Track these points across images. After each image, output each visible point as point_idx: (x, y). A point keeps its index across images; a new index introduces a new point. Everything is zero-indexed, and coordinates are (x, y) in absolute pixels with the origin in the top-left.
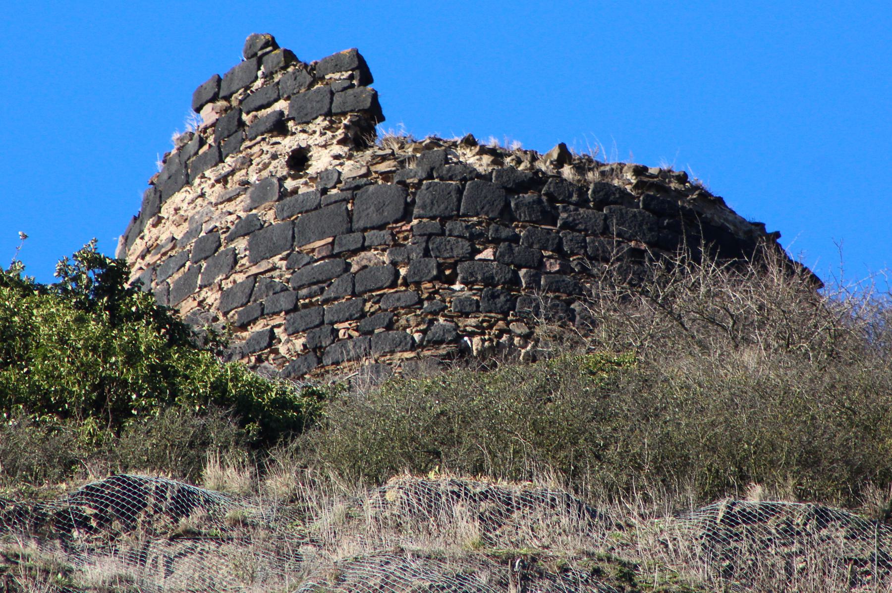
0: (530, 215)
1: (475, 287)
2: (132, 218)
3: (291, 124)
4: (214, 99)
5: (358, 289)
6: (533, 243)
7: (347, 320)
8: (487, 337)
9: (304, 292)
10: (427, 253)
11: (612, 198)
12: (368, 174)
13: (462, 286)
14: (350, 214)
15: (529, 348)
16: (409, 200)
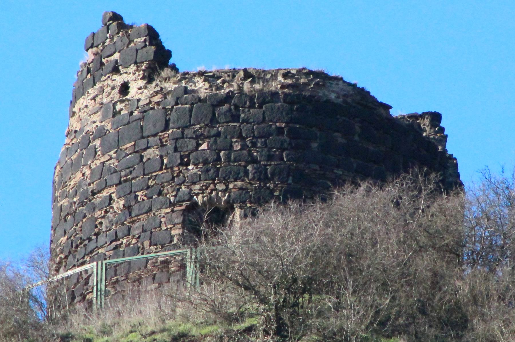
0: (226, 119)
1: (199, 167)
2: (70, 102)
3: (120, 68)
4: (92, 47)
5: (146, 172)
6: (227, 135)
7: (141, 190)
8: (205, 195)
9: (123, 173)
10: (176, 150)
11: (267, 100)
12: (150, 102)
13: (193, 166)
14: (142, 127)
15: (226, 197)
16: (167, 119)
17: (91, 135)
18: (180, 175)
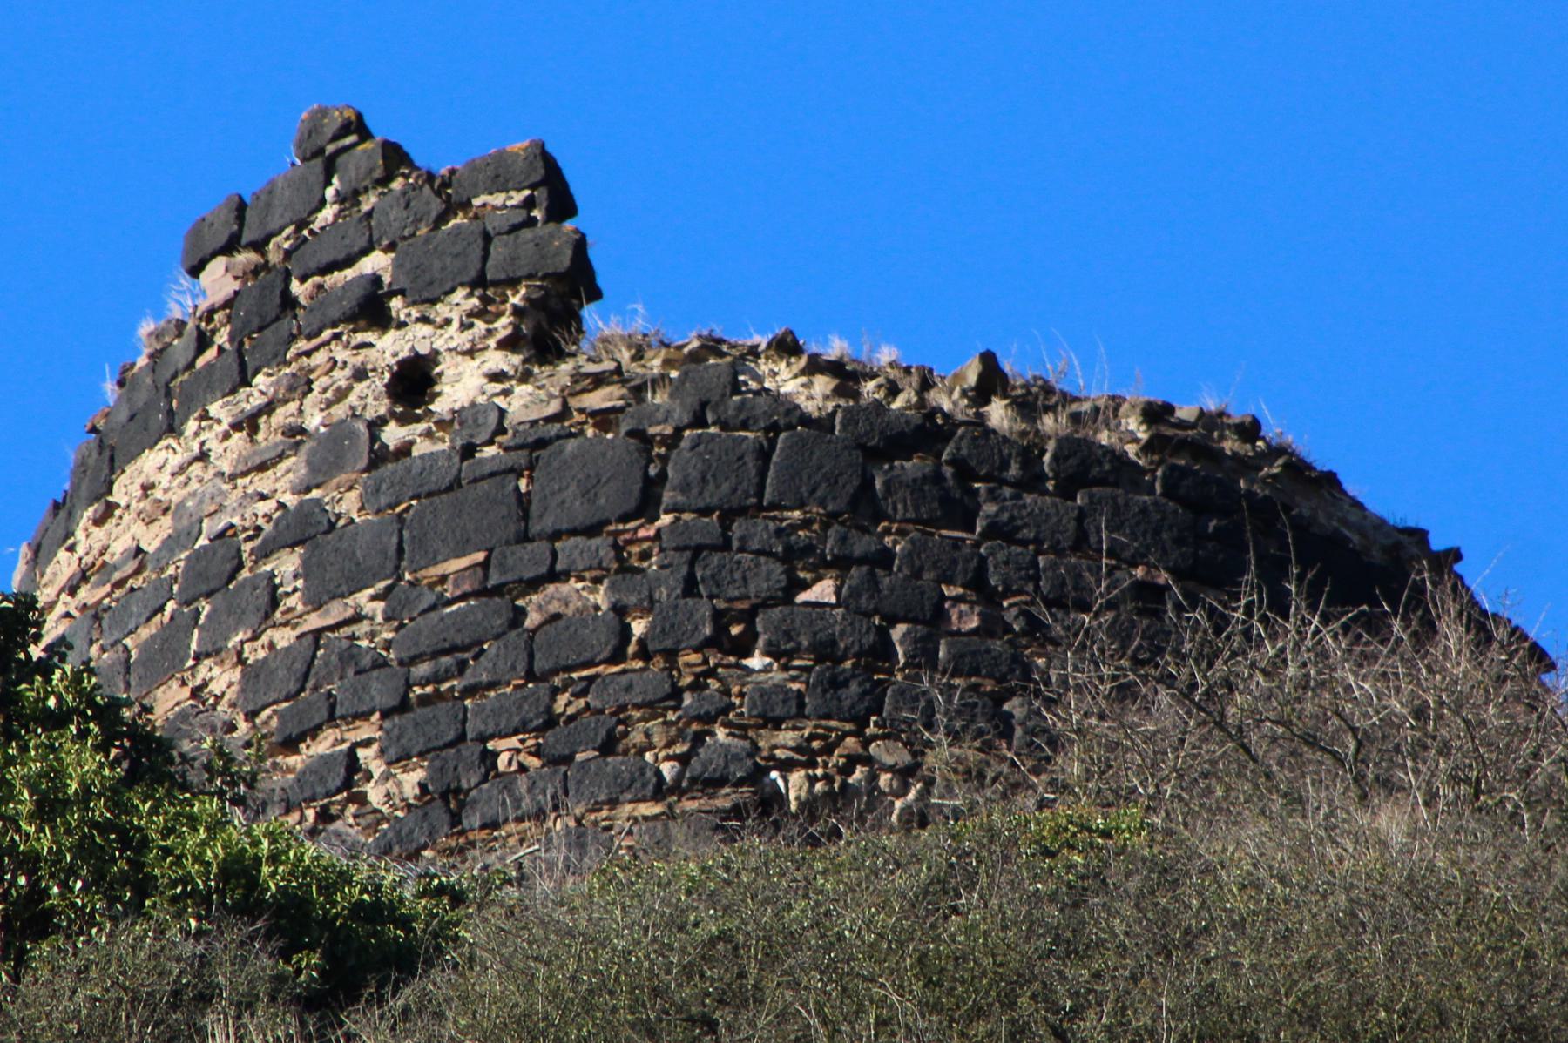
0: (917, 509)
1: (797, 663)
3: (396, 303)
5: (540, 664)
6: (921, 569)
7: (516, 732)
8: (819, 772)
9: (423, 669)
10: (690, 587)
11: (1095, 471)
12: (564, 414)
14: (523, 501)
15: (911, 796)
16: (652, 471)
17: (249, 538)
18: (707, 686)
